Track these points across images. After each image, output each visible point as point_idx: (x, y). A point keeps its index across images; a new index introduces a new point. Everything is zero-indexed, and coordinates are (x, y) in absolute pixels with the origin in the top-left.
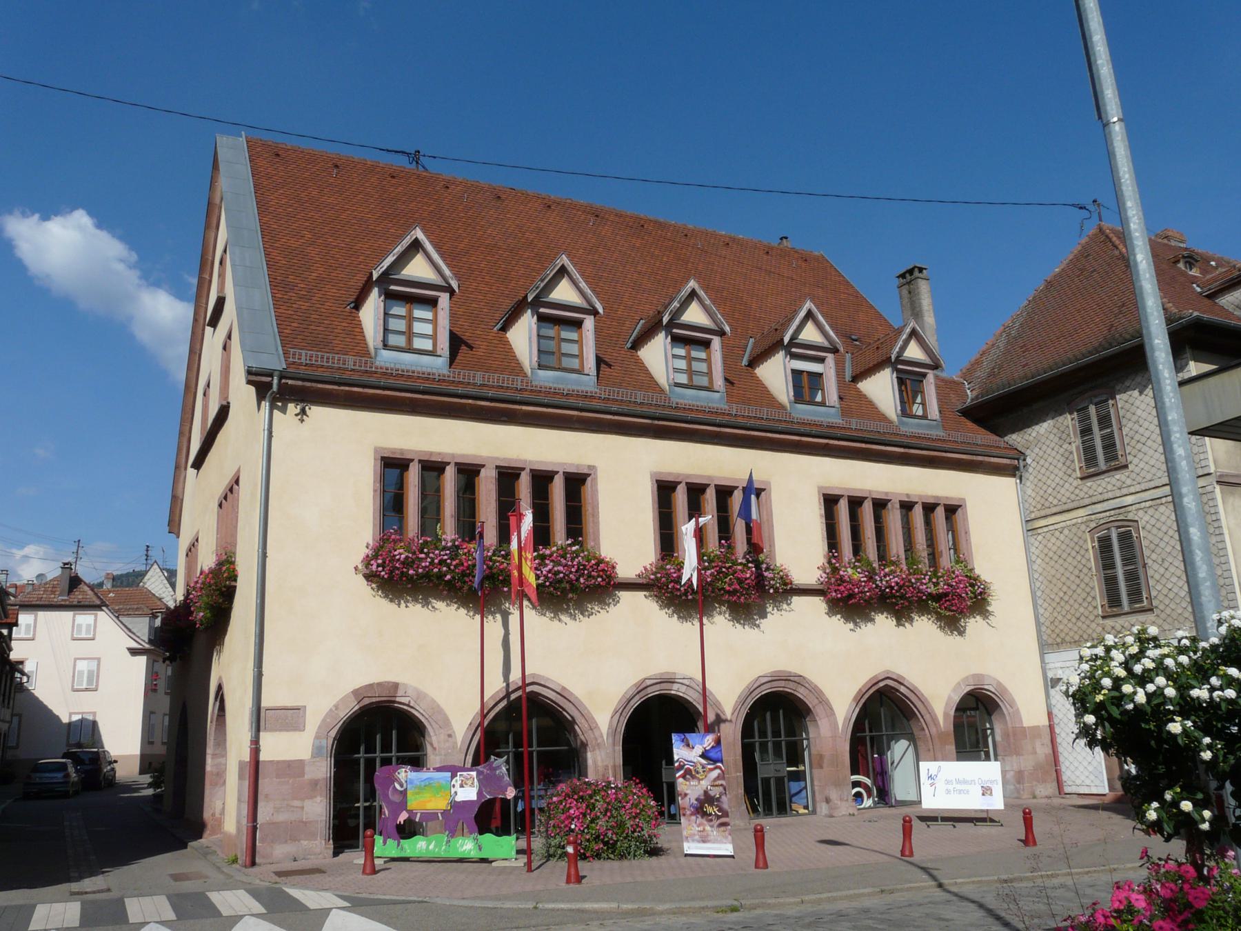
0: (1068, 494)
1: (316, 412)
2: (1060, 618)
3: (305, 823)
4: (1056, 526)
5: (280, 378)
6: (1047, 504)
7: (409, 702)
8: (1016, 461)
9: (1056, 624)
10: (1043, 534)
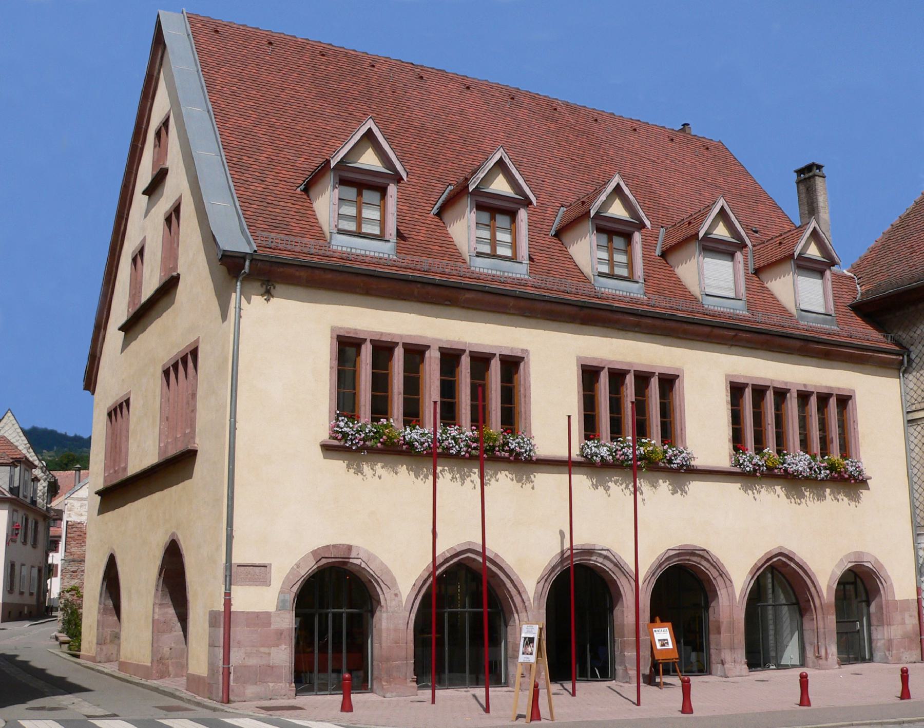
3: (272, 667)
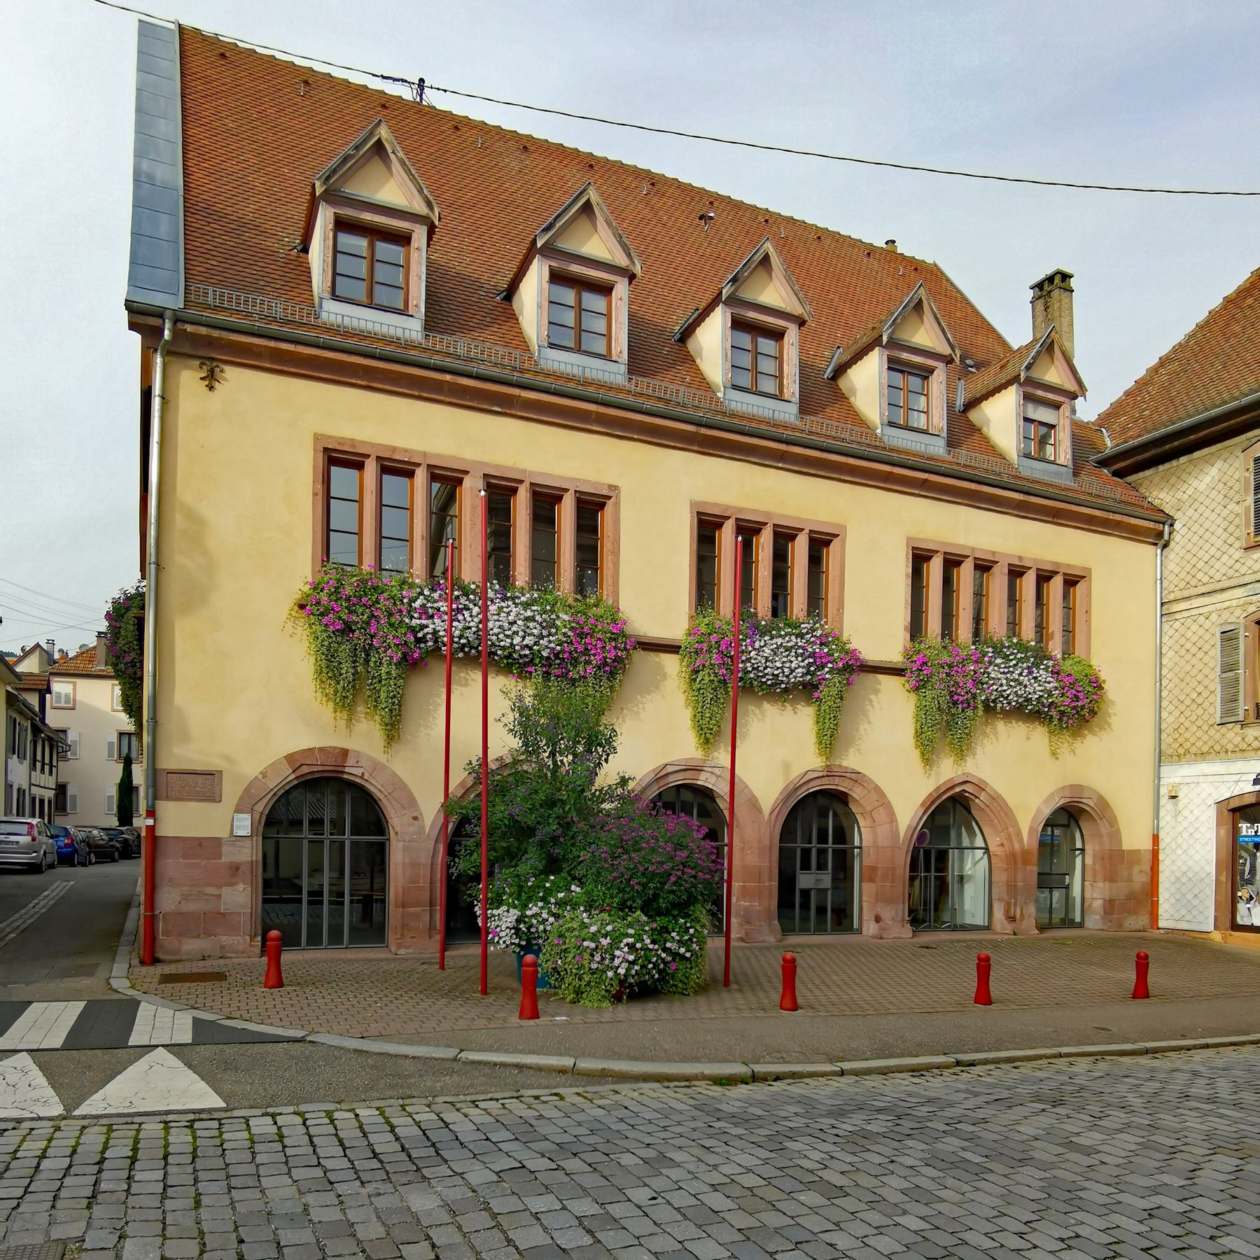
0: (1223, 570)
1: (234, 377)
2: (1187, 724)
3: (224, 915)
4: (1201, 610)
5: (176, 320)
6: (1193, 582)
7: (363, 774)
8: (1161, 525)
9: (1181, 731)
10: (1182, 621)
